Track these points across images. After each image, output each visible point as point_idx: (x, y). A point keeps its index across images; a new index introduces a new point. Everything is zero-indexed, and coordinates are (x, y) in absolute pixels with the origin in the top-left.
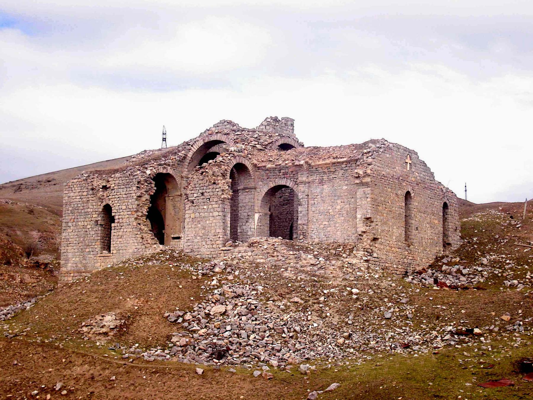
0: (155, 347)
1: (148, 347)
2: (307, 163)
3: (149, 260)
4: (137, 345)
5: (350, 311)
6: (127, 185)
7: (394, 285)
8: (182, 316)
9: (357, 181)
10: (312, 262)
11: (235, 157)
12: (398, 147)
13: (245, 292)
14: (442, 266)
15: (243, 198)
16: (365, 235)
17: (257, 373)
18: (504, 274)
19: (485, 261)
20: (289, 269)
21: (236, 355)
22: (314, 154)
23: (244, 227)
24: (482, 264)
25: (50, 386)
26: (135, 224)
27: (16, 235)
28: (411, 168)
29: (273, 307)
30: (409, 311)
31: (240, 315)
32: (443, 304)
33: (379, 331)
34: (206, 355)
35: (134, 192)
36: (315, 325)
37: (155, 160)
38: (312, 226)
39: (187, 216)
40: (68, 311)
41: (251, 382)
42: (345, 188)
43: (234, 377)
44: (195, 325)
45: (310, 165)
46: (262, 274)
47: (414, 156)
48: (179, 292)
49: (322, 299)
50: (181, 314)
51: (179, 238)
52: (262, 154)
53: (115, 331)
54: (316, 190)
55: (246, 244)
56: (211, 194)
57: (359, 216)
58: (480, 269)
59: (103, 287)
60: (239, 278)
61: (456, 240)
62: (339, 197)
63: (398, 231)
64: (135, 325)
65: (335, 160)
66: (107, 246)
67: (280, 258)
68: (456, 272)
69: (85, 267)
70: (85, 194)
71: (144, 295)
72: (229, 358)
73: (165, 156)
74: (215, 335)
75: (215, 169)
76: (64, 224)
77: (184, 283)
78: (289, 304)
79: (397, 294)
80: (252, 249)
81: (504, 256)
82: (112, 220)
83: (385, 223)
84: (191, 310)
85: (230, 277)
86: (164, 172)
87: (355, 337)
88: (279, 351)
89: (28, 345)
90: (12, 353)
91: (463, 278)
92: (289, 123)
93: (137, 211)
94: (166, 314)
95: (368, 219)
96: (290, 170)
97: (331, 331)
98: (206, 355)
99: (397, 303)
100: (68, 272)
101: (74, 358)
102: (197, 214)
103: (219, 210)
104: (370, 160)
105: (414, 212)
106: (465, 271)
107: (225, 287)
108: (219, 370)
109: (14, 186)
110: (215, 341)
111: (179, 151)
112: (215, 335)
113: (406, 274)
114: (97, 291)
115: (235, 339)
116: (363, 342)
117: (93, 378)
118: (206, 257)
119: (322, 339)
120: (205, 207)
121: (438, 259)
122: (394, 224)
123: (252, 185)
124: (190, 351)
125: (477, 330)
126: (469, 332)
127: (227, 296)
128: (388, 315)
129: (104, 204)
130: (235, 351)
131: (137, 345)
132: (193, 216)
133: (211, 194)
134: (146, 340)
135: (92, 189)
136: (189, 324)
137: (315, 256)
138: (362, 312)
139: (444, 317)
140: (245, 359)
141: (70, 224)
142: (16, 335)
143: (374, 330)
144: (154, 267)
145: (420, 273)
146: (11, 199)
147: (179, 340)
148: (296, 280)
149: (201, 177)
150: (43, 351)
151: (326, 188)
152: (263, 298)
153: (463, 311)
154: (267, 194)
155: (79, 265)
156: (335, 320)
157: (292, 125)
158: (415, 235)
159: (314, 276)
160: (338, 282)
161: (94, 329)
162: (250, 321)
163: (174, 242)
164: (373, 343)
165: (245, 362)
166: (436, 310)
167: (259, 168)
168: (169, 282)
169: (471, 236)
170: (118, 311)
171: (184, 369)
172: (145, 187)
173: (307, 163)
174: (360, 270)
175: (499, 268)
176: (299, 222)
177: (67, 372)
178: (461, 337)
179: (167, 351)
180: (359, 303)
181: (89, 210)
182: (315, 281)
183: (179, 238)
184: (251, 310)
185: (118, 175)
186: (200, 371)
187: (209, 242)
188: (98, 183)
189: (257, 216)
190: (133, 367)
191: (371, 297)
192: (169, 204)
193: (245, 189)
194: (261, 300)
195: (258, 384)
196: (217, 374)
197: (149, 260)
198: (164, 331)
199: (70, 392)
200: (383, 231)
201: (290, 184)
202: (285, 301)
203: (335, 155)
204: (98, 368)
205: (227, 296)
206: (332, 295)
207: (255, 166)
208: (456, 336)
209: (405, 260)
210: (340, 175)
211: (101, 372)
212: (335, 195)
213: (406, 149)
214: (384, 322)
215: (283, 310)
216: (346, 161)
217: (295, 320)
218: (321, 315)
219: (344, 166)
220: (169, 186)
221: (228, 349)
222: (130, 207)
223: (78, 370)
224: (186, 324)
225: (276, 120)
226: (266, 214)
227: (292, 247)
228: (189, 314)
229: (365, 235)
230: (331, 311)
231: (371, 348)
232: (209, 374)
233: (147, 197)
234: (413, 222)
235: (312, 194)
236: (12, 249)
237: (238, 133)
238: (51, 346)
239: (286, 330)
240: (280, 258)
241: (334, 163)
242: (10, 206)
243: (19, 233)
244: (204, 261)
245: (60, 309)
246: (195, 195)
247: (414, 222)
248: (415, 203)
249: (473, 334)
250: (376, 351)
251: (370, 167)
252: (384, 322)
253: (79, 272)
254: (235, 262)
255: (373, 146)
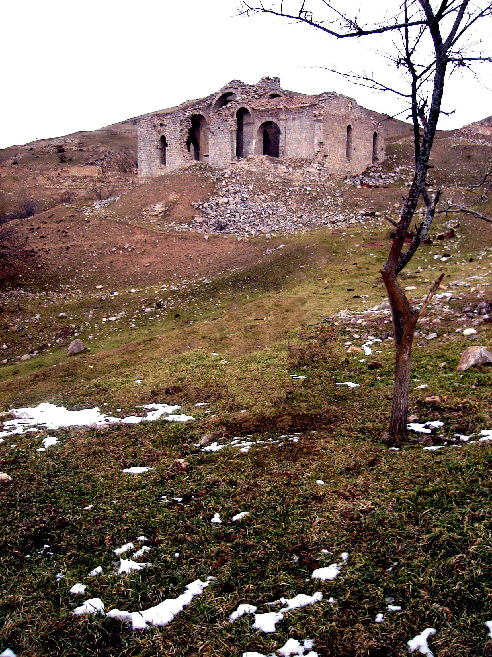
0: (185, 223)
1: (181, 223)
2: (284, 107)
3: (187, 170)
4: (174, 222)
5: (304, 202)
6: (174, 123)
7: (333, 185)
8: (202, 205)
9: (315, 119)
10: (285, 171)
11: (239, 103)
12: (342, 96)
13: (241, 190)
14: (370, 173)
15: (246, 129)
16: (319, 154)
17: (239, 239)
18: (407, 178)
19: (397, 170)
20: (271, 175)
21: (231, 228)
22: (290, 101)
23: (247, 149)
24: (395, 172)
25: (122, 246)
26: (179, 147)
27: (130, 153)
28: (351, 110)
29: (257, 199)
30: (339, 202)
31: (237, 204)
32: (362, 197)
33: (319, 214)
34: (214, 228)
35: (178, 127)
36: (281, 210)
37: (192, 106)
38: (288, 148)
39: (210, 142)
40: (137, 202)
41: (235, 244)
42: (308, 123)
43: (226, 241)
44: (209, 210)
45: (287, 108)
46: (253, 178)
47: (354, 102)
48: (202, 190)
49: (288, 194)
50: (201, 203)
51: (208, 156)
52: (258, 101)
53: (162, 214)
54: (291, 124)
55: (246, 160)
56: (224, 128)
57: (316, 141)
58: (393, 175)
59: (157, 187)
60: (239, 181)
61: (382, 156)
62: (305, 129)
63: (342, 151)
64: (174, 210)
65: (302, 105)
66: (163, 161)
67: (266, 168)
68: (378, 177)
69: (152, 175)
70: (150, 129)
71: (180, 192)
72: (227, 229)
73: (198, 103)
74: (221, 216)
75: (227, 112)
76: (138, 149)
77: (205, 184)
78: (267, 197)
79: (334, 190)
80: (249, 162)
81: (410, 167)
82: (166, 145)
83: (333, 146)
84: (208, 201)
85: (234, 181)
86: (198, 113)
87: (304, 217)
88: (257, 226)
89: (111, 222)
90: (102, 227)
91: (381, 181)
92: (277, 80)
93: (181, 139)
94: (193, 204)
95: (321, 143)
96: (275, 111)
97: (290, 213)
98: (214, 228)
99: (334, 196)
100: (142, 178)
101: (136, 230)
102: (216, 141)
103: (229, 138)
104: (323, 105)
105: (353, 139)
106: (383, 176)
107: (230, 187)
108: (218, 237)
109: (132, 121)
110: (220, 220)
111: (207, 100)
112: (221, 216)
113: (346, 178)
114: (153, 190)
115: (232, 219)
116: (308, 220)
117: (146, 242)
118: (221, 168)
119: (284, 218)
120: (220, 136)
121: (368, 168)
122: (338, 146)
123: (251, 121)
124: (205, 225)
125: (377, 213)
126: (373, 214)
127: (230, 192)
128: (326, 204)
129: (161, 135)
130: (231, 226)
131: (174, 222)
132: (213, 142)
133: (224, 128)
134: (179, 219)
135: (154, 126)
136: (206, 209)
137: (287, 167)
138: (311, 202)
139: (360, 205)
140: (236, 230)
141: (142, 148)
142: (107, 217)
143: (317, 213)
144: (188, 174)
145: (355, 177)
146: (128, 130)
147: (199, 219)
148: (274, 182)
149: (218, 117)
150: (119, 226)
151: (297, 123)
152: (252, 193)
153: (372, 202)
154: (260, 127)
155: (148, 174)
156: (294, 207)
157: (279, 82)
158: (354, 153)
159: (285, 179)
160: (300, 183)
161: (150, 213)
162: (242, 208)
163: (205, 159)
164: (314, 221)
165: (236, 232)
166: (356, 201)
167: (256, 110)
168: (196, 183)
169: (393, 154)
170: (165, 202)
171: (198, 237)
172: (185, 124)
173: (284, 107)
174: (314, 175)
175: (405, 174)
176: (280, 145)
177: (132, 238)
178: (367, 217)
179: (191, 226)
180: (310, 196)
181: (153, 139)
182: (286, 183)
183: (208, 156)
184: (244, 201)
185: (169, 116)
186: (206, 237)
187: (223, 158)
188: (158, 122)
189: (254, 141)
190: (168, 235)
191: (318, 193)
192: (202, 134)
193: (247, 124)
194: (251, 195)
195: (240, 245)
196: (216, 239)
197: (187, 170)
198: (191, 213)
199: (133, 249)
200: (331, 151)
201: (275, 120)
202: (265, 195)
203: (302, 102)
204: (149, 236)
205: (230, 192)
206: (294, 191)
207: (253, 109)
208: (364, 217)
209: (346, 169)
210: (305, 114)
211: (151, 238)
212: (302, 127)
213: (348, 98)
214: (323, 208)
215: (263, 201)
216: (309, 106)
217: (270, 207)
218: (286, 203)
219: (307, 109)
220: (202, 123)
221: (227, 225)
222: (176, 137)
223: (138, 237)
224: (204, 210)
225: (268, 78)
226: (260, 140)
227: (272, 161)
228: (206, 203)
229: (319, 154)
230: (292, 202)
231: (313, 224)
232: (212, 239)
233: (187, 130)
234: (352, 145)
235: (288, 127)
236: (128, 162)
237: (244, 88)
238: (124, 223)
239: (263, 213)
240: (266, 168)
241: (301, 107)
242: (127, 135)
243: (132, 152)
244: (220, 170)
245: (132, 201)
246: (215, 129)
247: (352, 145)
248: (354, 133)
249: (375, 216)
250: (315, 226)
251: (323, 109)
252: (323, 208)
253: (148, 178)
254: (238, 171)
255: (326, 96)
